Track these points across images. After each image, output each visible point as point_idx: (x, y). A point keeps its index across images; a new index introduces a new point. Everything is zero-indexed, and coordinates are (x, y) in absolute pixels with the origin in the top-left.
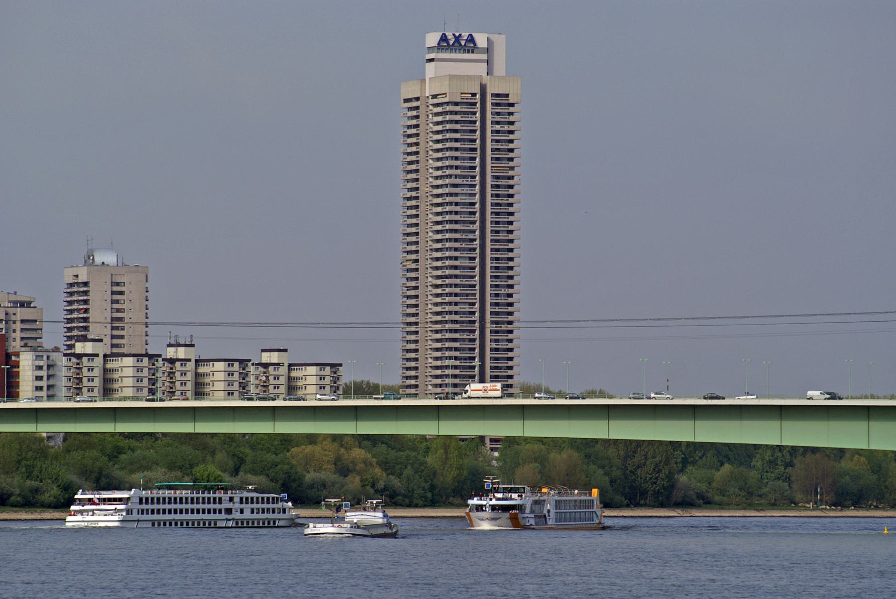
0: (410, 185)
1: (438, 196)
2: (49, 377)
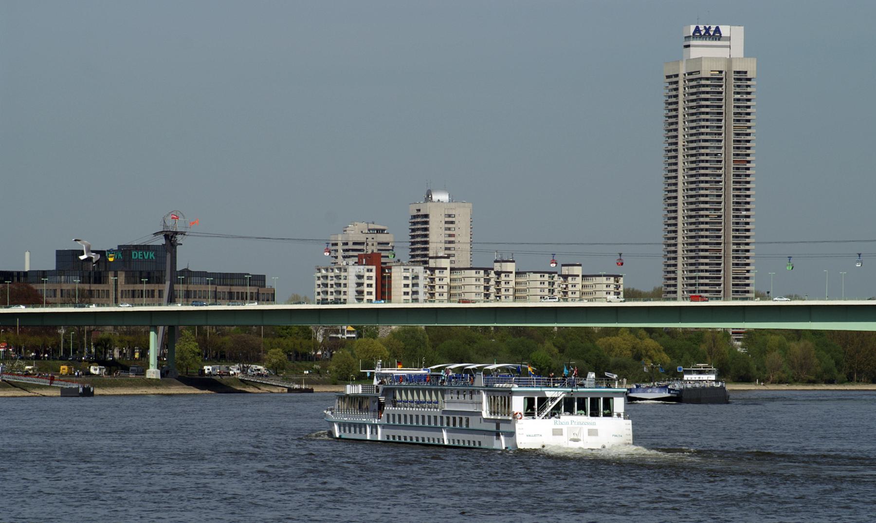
0: (670, 141)
1: (692, 149)
2: (413, 285)
